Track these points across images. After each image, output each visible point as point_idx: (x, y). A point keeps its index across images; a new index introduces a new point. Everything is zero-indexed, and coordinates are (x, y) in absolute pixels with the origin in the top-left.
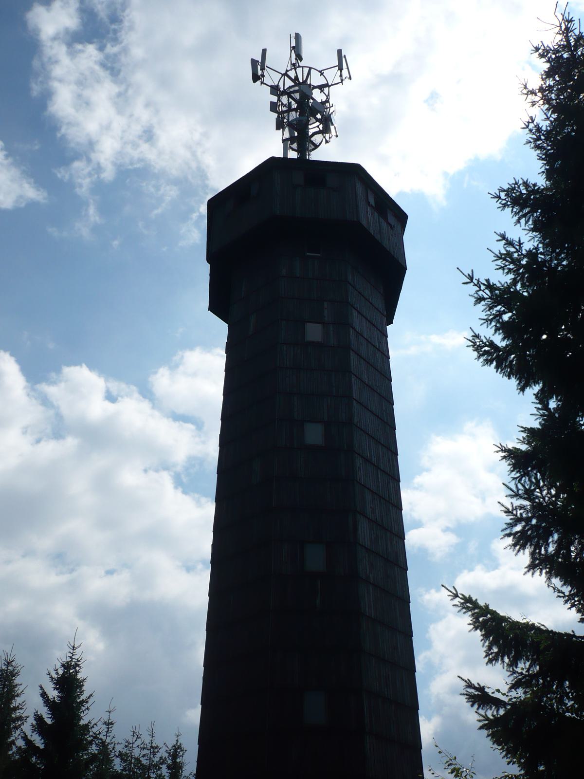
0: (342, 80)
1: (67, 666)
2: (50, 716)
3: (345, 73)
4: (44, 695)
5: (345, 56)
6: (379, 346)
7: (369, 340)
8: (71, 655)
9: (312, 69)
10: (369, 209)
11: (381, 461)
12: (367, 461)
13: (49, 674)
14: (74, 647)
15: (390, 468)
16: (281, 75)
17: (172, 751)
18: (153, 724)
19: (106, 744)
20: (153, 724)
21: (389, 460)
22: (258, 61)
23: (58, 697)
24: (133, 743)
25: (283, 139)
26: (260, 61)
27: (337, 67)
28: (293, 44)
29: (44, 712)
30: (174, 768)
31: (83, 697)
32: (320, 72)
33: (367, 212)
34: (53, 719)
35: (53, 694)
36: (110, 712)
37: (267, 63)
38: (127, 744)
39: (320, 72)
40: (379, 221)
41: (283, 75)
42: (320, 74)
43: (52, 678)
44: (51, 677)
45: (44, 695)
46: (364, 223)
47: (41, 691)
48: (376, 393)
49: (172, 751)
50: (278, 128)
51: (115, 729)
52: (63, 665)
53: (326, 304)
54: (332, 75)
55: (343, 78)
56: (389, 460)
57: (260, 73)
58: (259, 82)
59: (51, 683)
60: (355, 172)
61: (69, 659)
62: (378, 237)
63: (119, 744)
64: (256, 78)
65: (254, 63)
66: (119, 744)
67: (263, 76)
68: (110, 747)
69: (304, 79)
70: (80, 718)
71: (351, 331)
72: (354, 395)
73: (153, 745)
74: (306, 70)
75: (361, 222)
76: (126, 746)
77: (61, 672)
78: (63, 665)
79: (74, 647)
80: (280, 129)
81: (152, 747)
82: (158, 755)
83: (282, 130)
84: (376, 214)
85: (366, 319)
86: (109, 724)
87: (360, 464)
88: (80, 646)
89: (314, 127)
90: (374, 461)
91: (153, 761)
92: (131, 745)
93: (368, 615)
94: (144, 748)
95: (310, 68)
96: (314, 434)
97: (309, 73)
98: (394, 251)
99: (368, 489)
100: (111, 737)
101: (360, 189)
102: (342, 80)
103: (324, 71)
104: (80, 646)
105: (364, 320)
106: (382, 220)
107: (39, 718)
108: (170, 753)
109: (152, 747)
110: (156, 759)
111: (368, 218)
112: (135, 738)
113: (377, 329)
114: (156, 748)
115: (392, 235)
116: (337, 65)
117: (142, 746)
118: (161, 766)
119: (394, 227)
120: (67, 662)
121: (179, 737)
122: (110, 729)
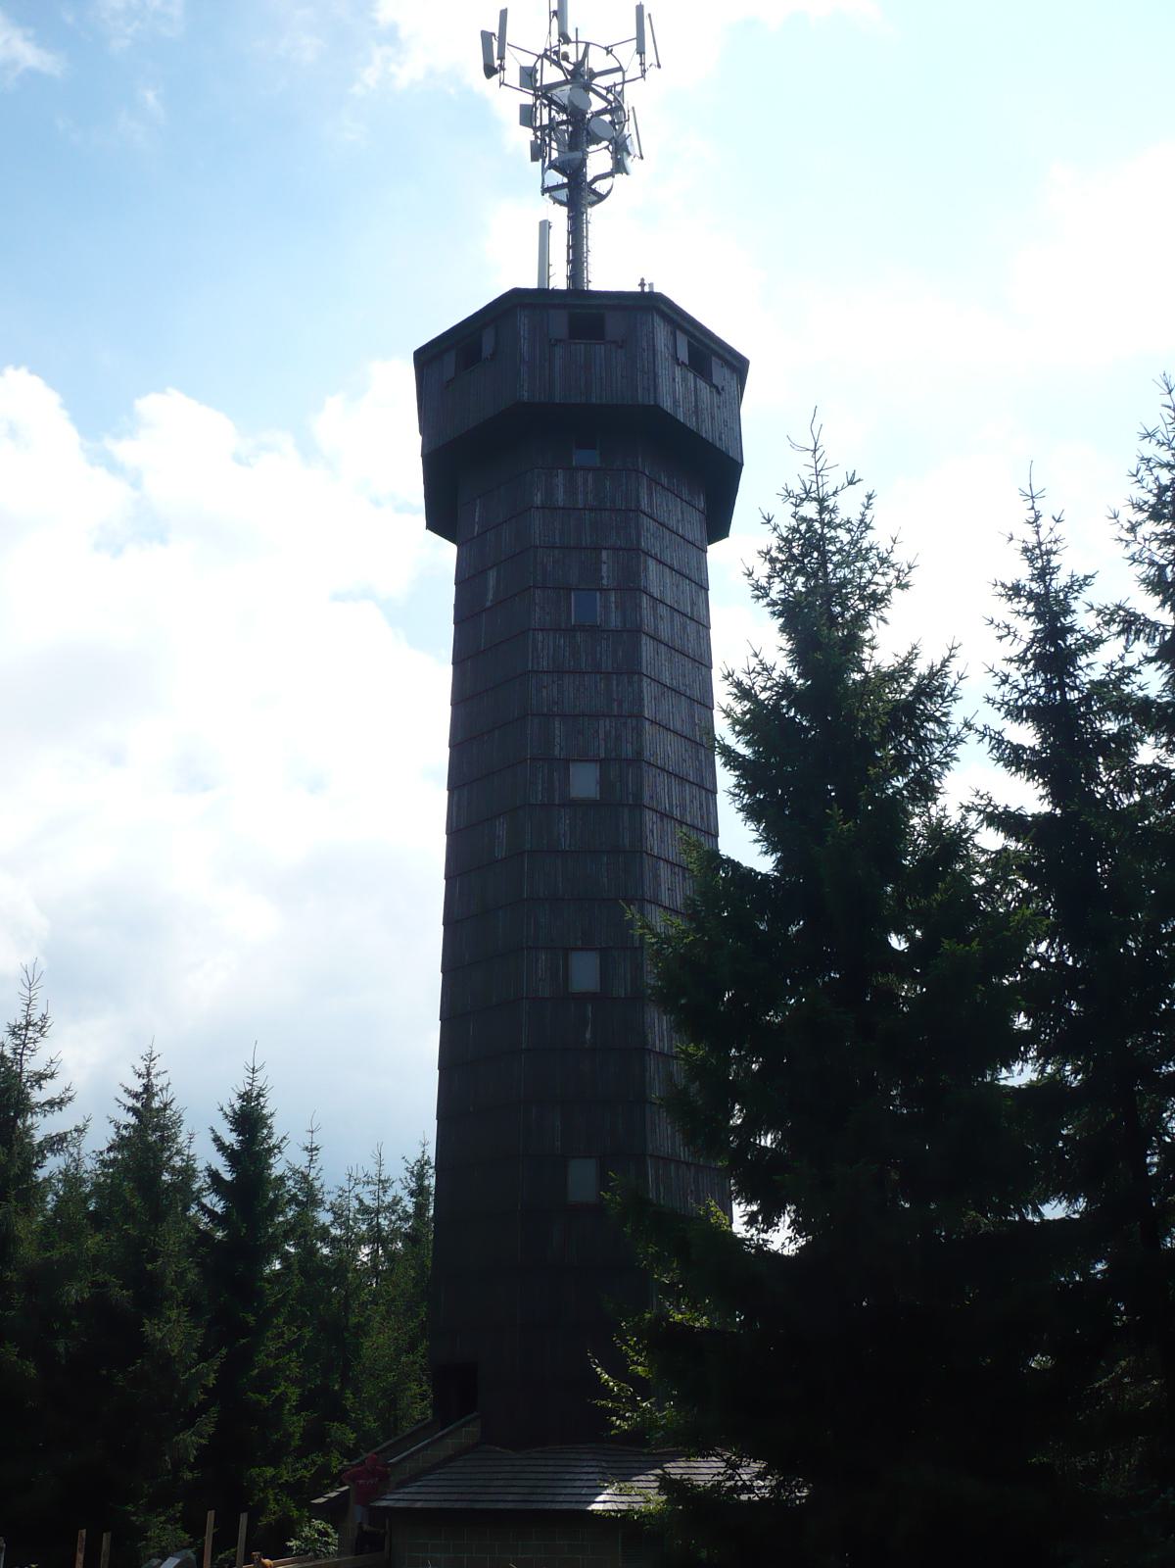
0: (644, 71)
1: (245, 1097)
2: (229, 1169)
3: (650, 57)
4: (217, 1139)
5: (649, 15)
6: (692, 613)
7: (676, 606)
8: (251, 1081)
9: (591, 46)
10: (678, 372)
11: (688, 810)
12: (664, 816)
13: (222, 1109)
14: (253, 1069)
15: (702, 818)
16: (536, 58)
17: (416, 1168)
18: (380, 1146)
19: (310, 1179)
20: (380, 1146)
21: (701, 805)
22: (494, 34)
23: (238, 1141)
24: (350, 1191)
25: (542, 187)
26: (497, 35)
27: (635, 41)
28: (555, 7)
29: (221, 1164)
30: (420, 1194)
31: (273, 1141)
32: (606, 49)
33: (674, 379)
34: (233, 1172)
35: (231, 1138)
36: (312, 1132)
37: (509, 39)
38: (340, 1193)
39: (606, 49)
40: (695, 387)
41: (539, 57)
42: (605, 52)
43: (226, 1116)
44: (225, 1114)
45: (217, 1139)
46: (667, 404)
47: (212, 1136)
48: (683, 697)
49: (416, 1168)
50: (534, 158)
51: (321, 1157)
52: (240, 1097)
53: (604, 554)
54: (627, 55)
55: (647, 66)
56: (701, 805)
57: (497, 63)
58: (496, 78)
59: (226, 1122)
60: (649, 306)
61: (248, 1088)
62: (691, 423)
63: (329, 1193)
64: (490, 71)
65: (486, 37)
66: (329, 1193)
67: (502, 68)
68: (317, 1184)
69: (580, 59)
70: (270, 1166)
71: (645, 598)
72: (646, 712)
73: (382, 1178)
74: (582, 47)
75: (661, 404)
76: (340, 1196)
77: (237, 1106)
78: (240, 1097)
79: (253, 1069)
80: (538, 160)
81: (379, 1181)
82: (391, 1192)
83: (541, 160)
84: (691, 376)
85: (671, 568)
86: (312, 1150)
87: (653, 823)
88: (262, 1067)
89: (598, 160)
90: (677, 813)
91: (383, 1201)
92: (347, 1194)
93: (658, 1050)
94: (368, 1183)
95: (588, 44)
96: (584, 782)
97: (586, 54)
98: (720, 439)
99: (665, 860)
100: (317, 1169)
101: (661, 333)
102: (644, 71)
103: (614, 48)
104: (262, 1067)
105: (667, 570)
106: (701, 384)
107: (214, 1175)
108: (412, 1172)
109: (379, 1181)
110: (388, 1199)
111: (675, 391)
112: (352, 1184)
113: (690, 580)
114: (386, 1181)
115: (719, 407)
116: (635, 36)
117: (365, 1179)
118: (395, 1208)
119: (723, 389)
120: (246, 1093)
121: (426, 1147)
122: (314, 1158)
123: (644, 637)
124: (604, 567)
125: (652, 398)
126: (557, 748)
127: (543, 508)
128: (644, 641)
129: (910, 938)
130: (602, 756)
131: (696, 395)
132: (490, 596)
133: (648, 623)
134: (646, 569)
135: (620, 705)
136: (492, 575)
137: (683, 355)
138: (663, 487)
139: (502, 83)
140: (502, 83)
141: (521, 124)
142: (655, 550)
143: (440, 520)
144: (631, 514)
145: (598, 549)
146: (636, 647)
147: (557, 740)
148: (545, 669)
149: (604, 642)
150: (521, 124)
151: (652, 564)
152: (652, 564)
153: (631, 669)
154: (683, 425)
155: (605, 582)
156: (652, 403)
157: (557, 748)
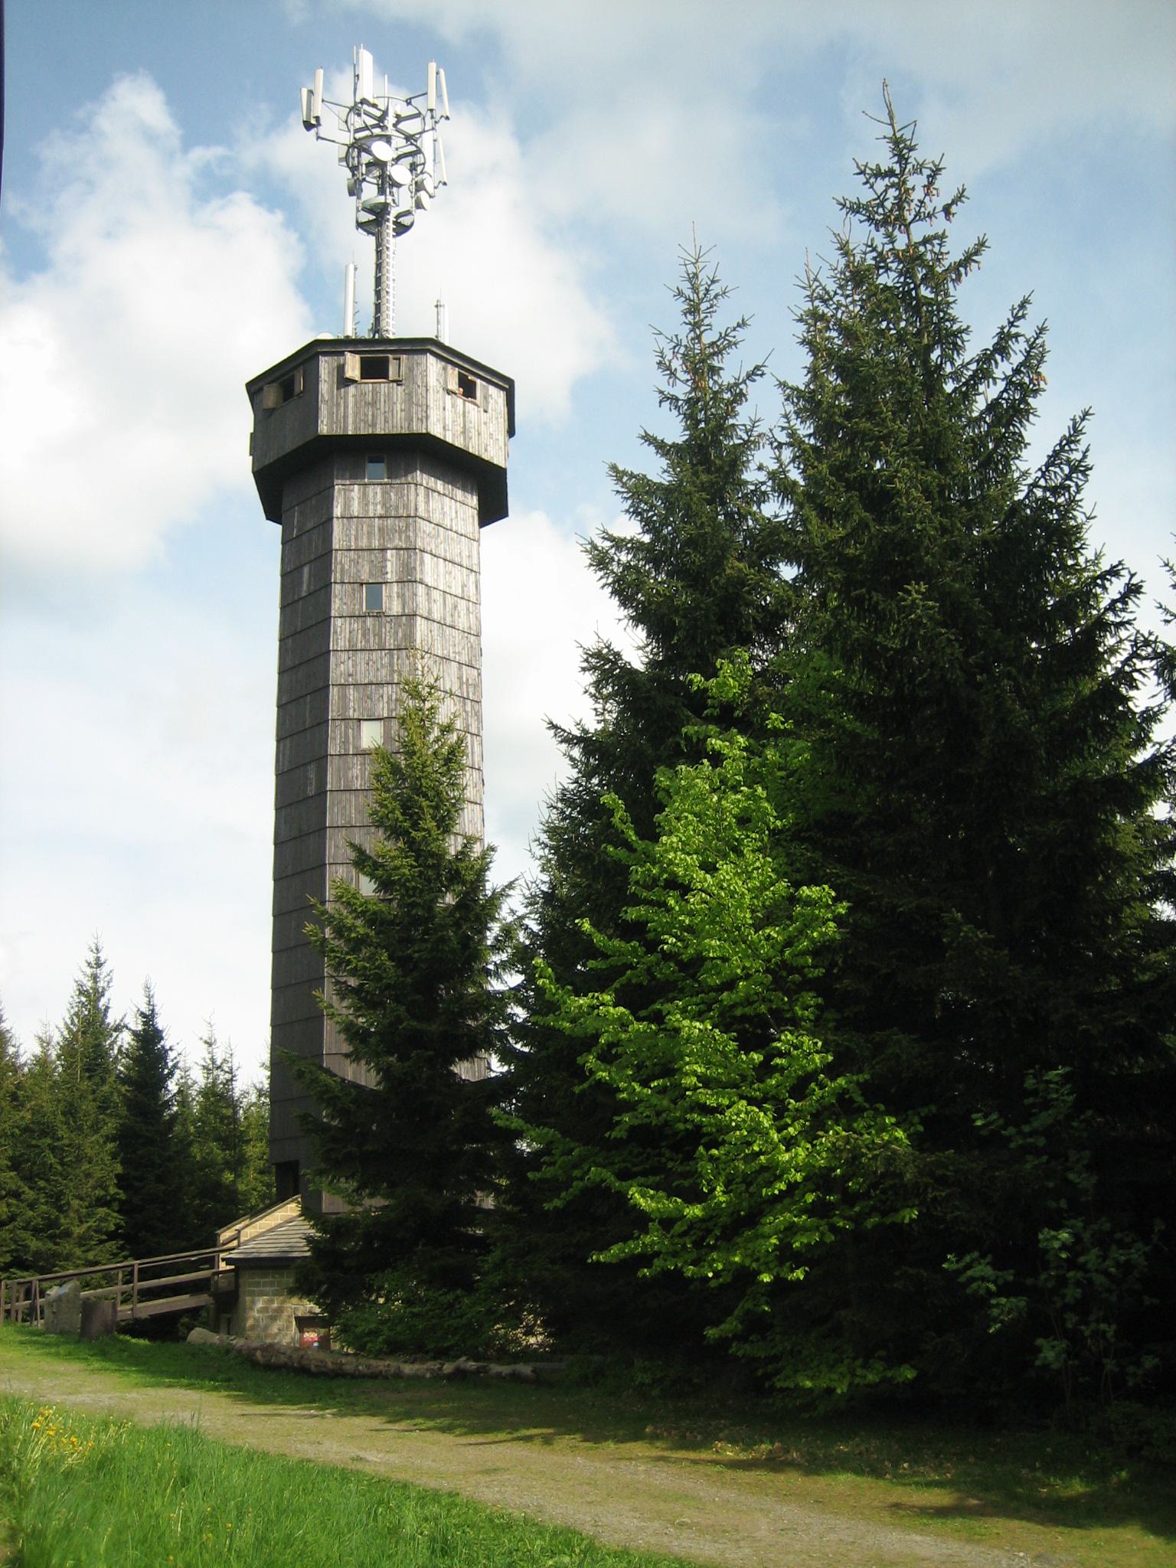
58: (314, 131)
62: (459, 443)
98: (486, 450)
123: (419, 618)
124: (389, 564)
125: (424, 426)
126: (351, 711)
127: (342, 518)
128: (418, 623)
129: (497, 1190)
130: (385, 715)
131: (464, 416)
132: (305, 587)
133: (423, 610)
134: (422, 562)
135: (400, 675)
136: (306, 570)
137: (453, 385)
138: (439, 493)
139: (318, 138)
140: (318, 138)
141: (255, 388)
142: (431, 547)
143: (273, 512)
144: (411, 520)
145: (384, 550)
146: (412, 627)
147: (352, 704)
148: (357, 613)
149: (388, 625)
150: (255, 388)
151: (427, 557)
152: (427, 557)
153: (407, 646)
154: (452, 445)
155: (389, 576)
156: (424, 431)
157: (351, 711)
